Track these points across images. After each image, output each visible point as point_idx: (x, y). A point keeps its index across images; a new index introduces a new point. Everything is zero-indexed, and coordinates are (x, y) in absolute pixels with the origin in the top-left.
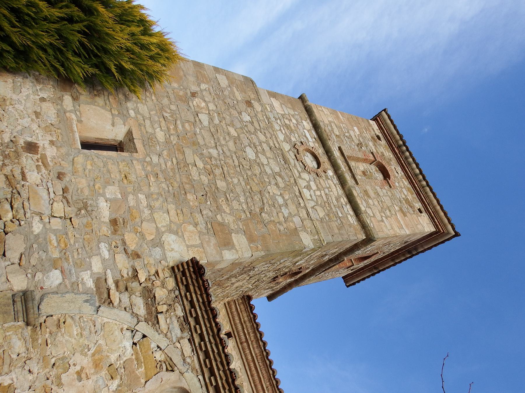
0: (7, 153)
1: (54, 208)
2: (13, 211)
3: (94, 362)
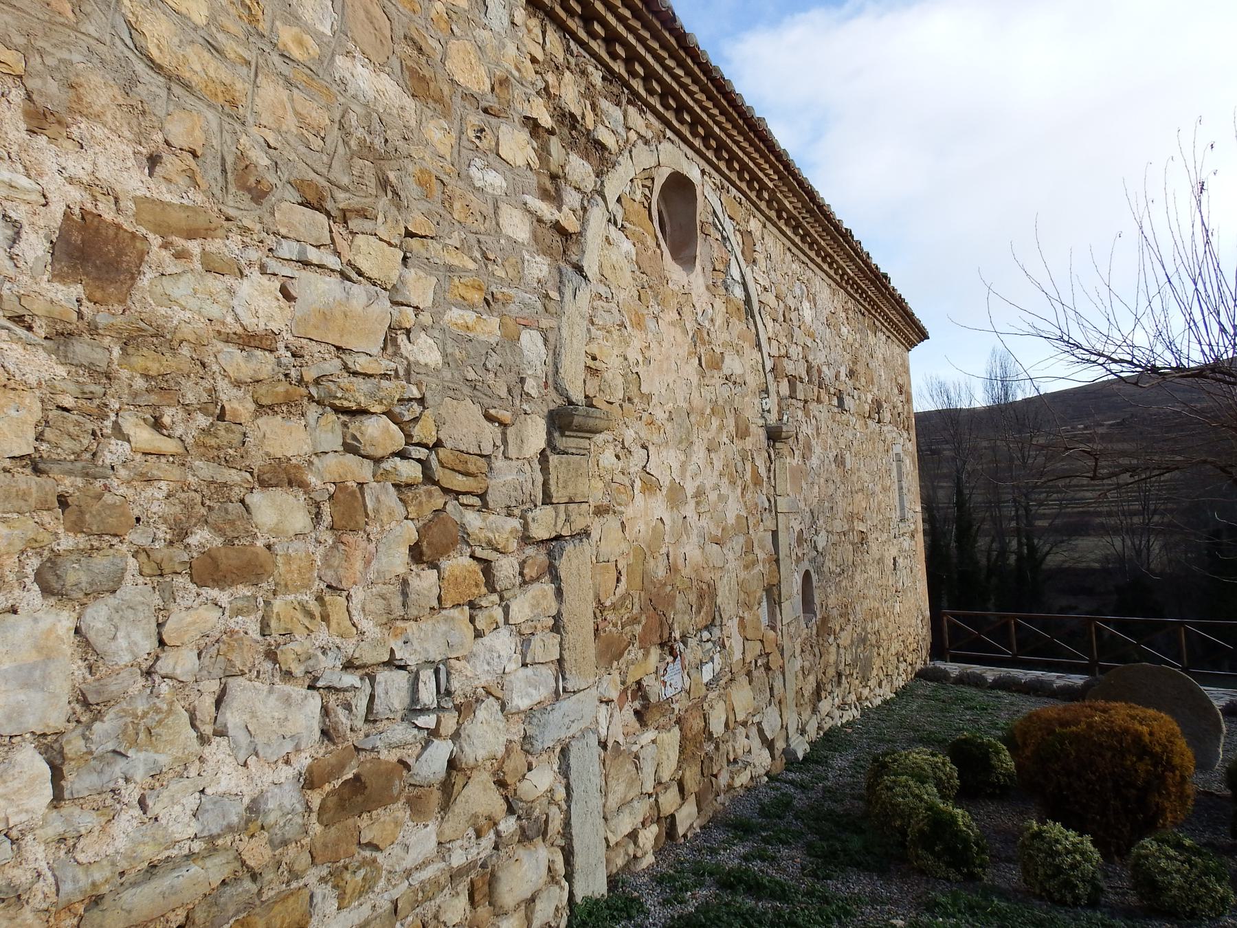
0: (140, 383)
1: (374, 274)
2: (372, 410)
3: (783, 891)
